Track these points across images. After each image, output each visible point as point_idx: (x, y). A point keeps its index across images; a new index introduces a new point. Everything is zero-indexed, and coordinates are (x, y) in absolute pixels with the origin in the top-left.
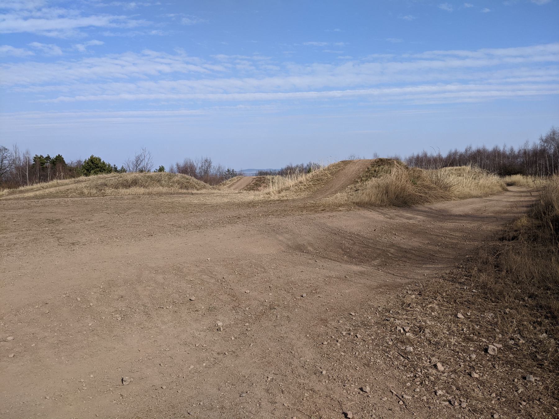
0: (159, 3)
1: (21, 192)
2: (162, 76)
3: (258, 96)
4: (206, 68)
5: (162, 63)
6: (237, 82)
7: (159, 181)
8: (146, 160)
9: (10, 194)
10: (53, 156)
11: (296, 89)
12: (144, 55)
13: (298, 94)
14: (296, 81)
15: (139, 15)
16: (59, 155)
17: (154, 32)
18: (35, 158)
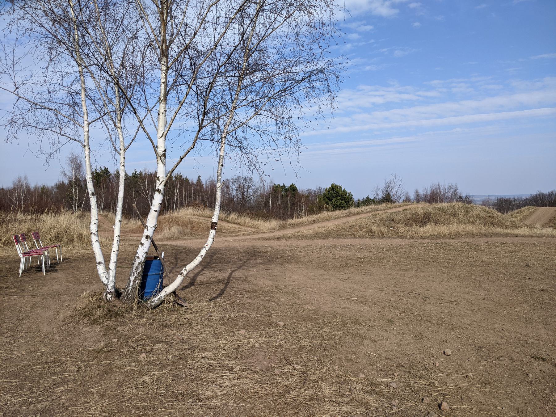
0: (372, 41)
1: (292, 226)
2: (376, 107)
3: (477, 117)
4: (419, 96)
5: (375, 96)
6: (453, 106)
7: (455, 215)
8: (396, 188)
9: (282, 228)
10: (287, 185)
11: (523, 107)
12: (359, 90)
13: (527, 112)
14: (523, 98)
15: (354, 54)
16: (20, 181)
17: (368, 68)
18: (273, 187)
